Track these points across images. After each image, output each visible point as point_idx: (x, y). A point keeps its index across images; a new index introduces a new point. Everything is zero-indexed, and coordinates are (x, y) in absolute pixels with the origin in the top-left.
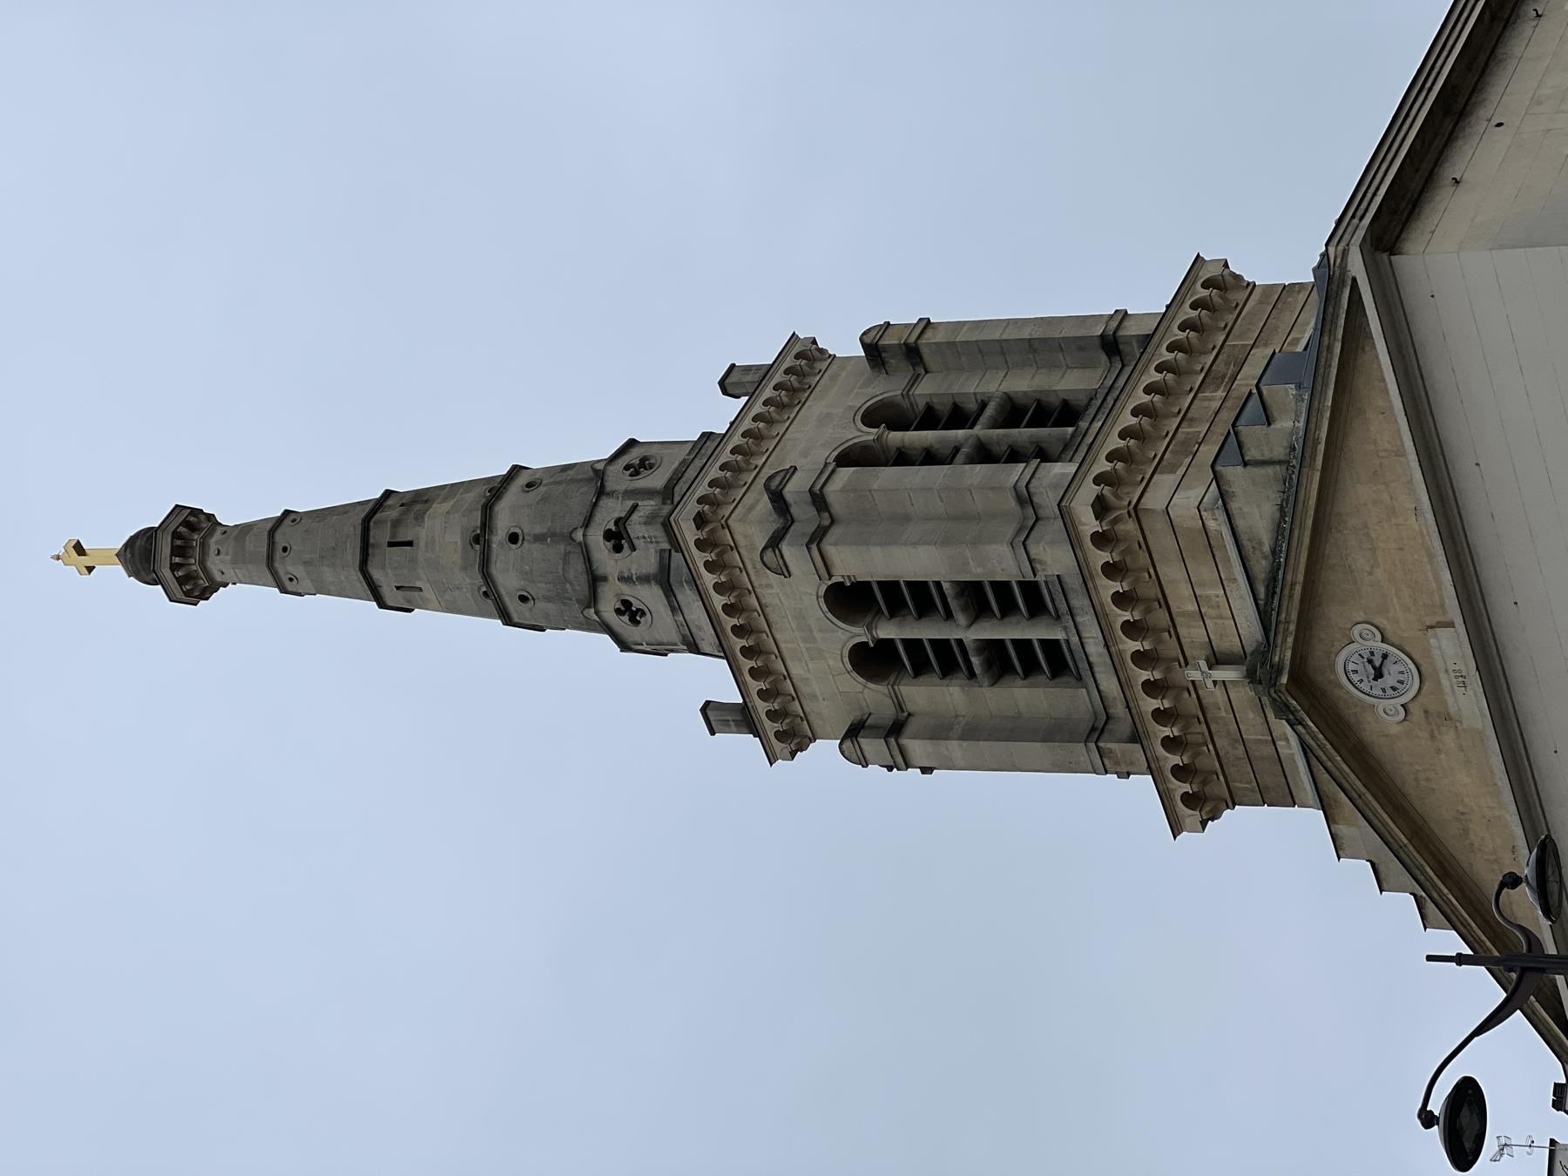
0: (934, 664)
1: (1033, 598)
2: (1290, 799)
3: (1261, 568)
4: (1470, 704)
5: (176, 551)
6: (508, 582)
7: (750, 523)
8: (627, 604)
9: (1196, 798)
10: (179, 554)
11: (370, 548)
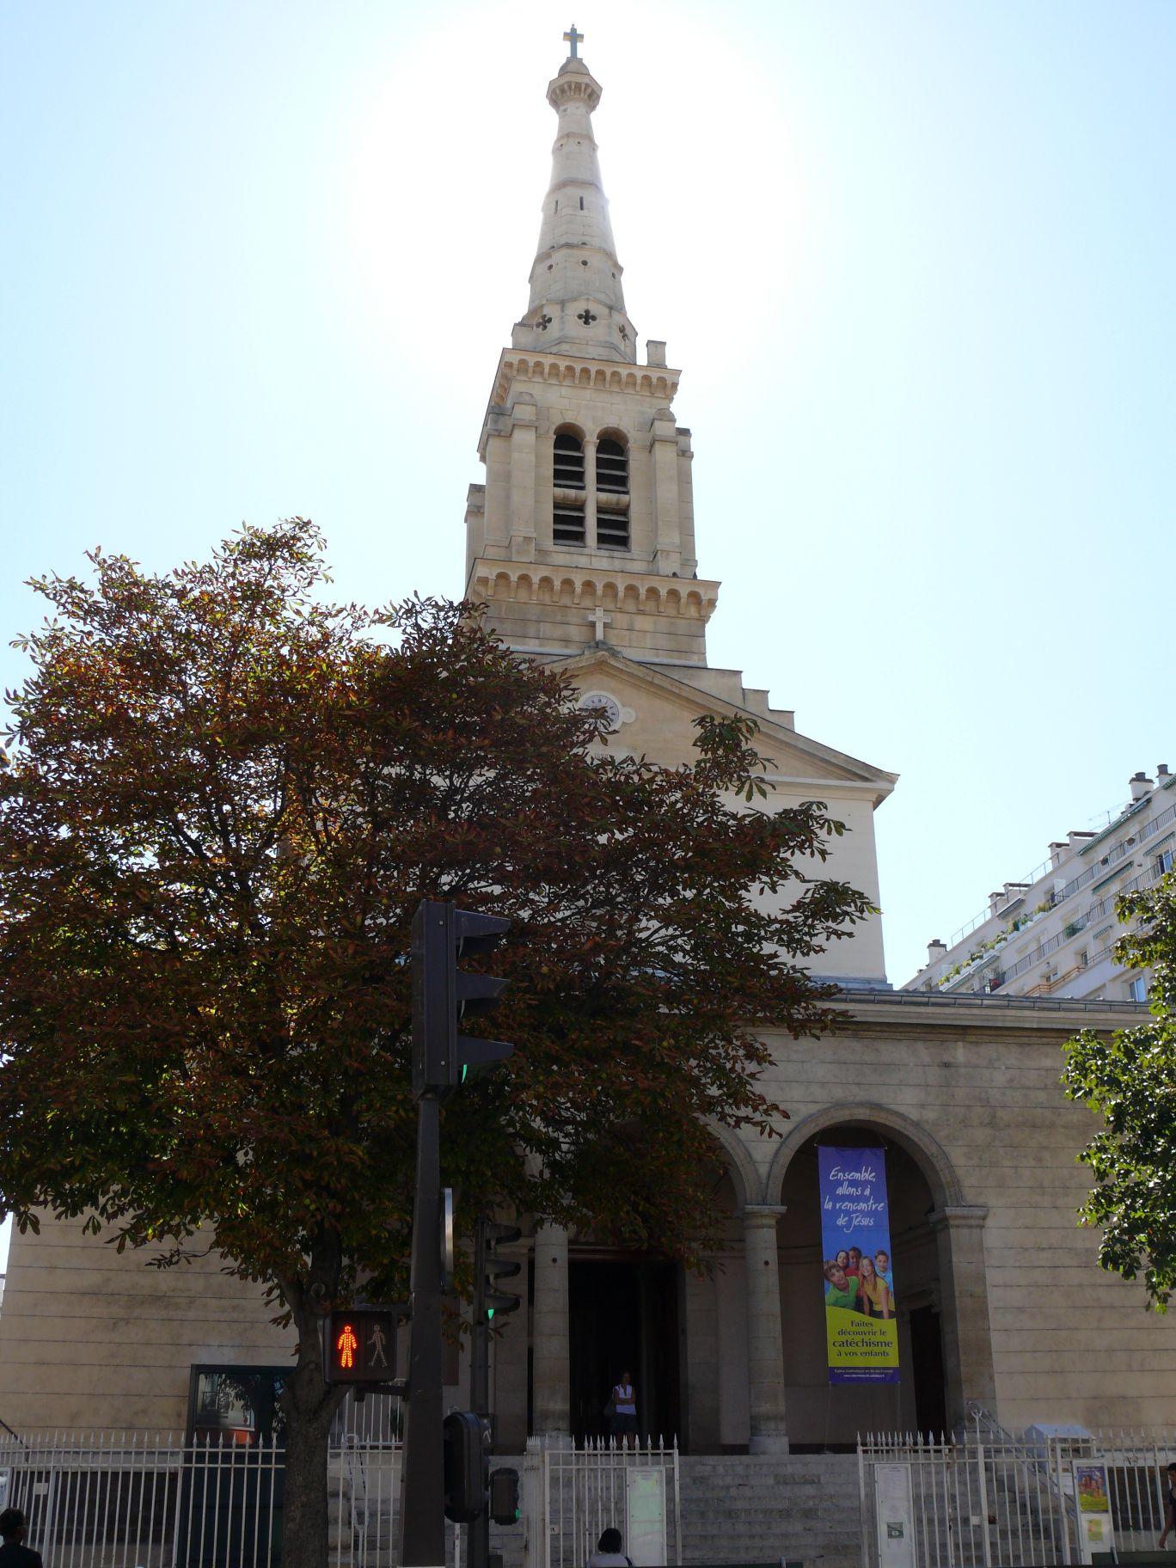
6: (558, 257)
8: (594, 318)
10: (574, 90)
11: (575, 186)
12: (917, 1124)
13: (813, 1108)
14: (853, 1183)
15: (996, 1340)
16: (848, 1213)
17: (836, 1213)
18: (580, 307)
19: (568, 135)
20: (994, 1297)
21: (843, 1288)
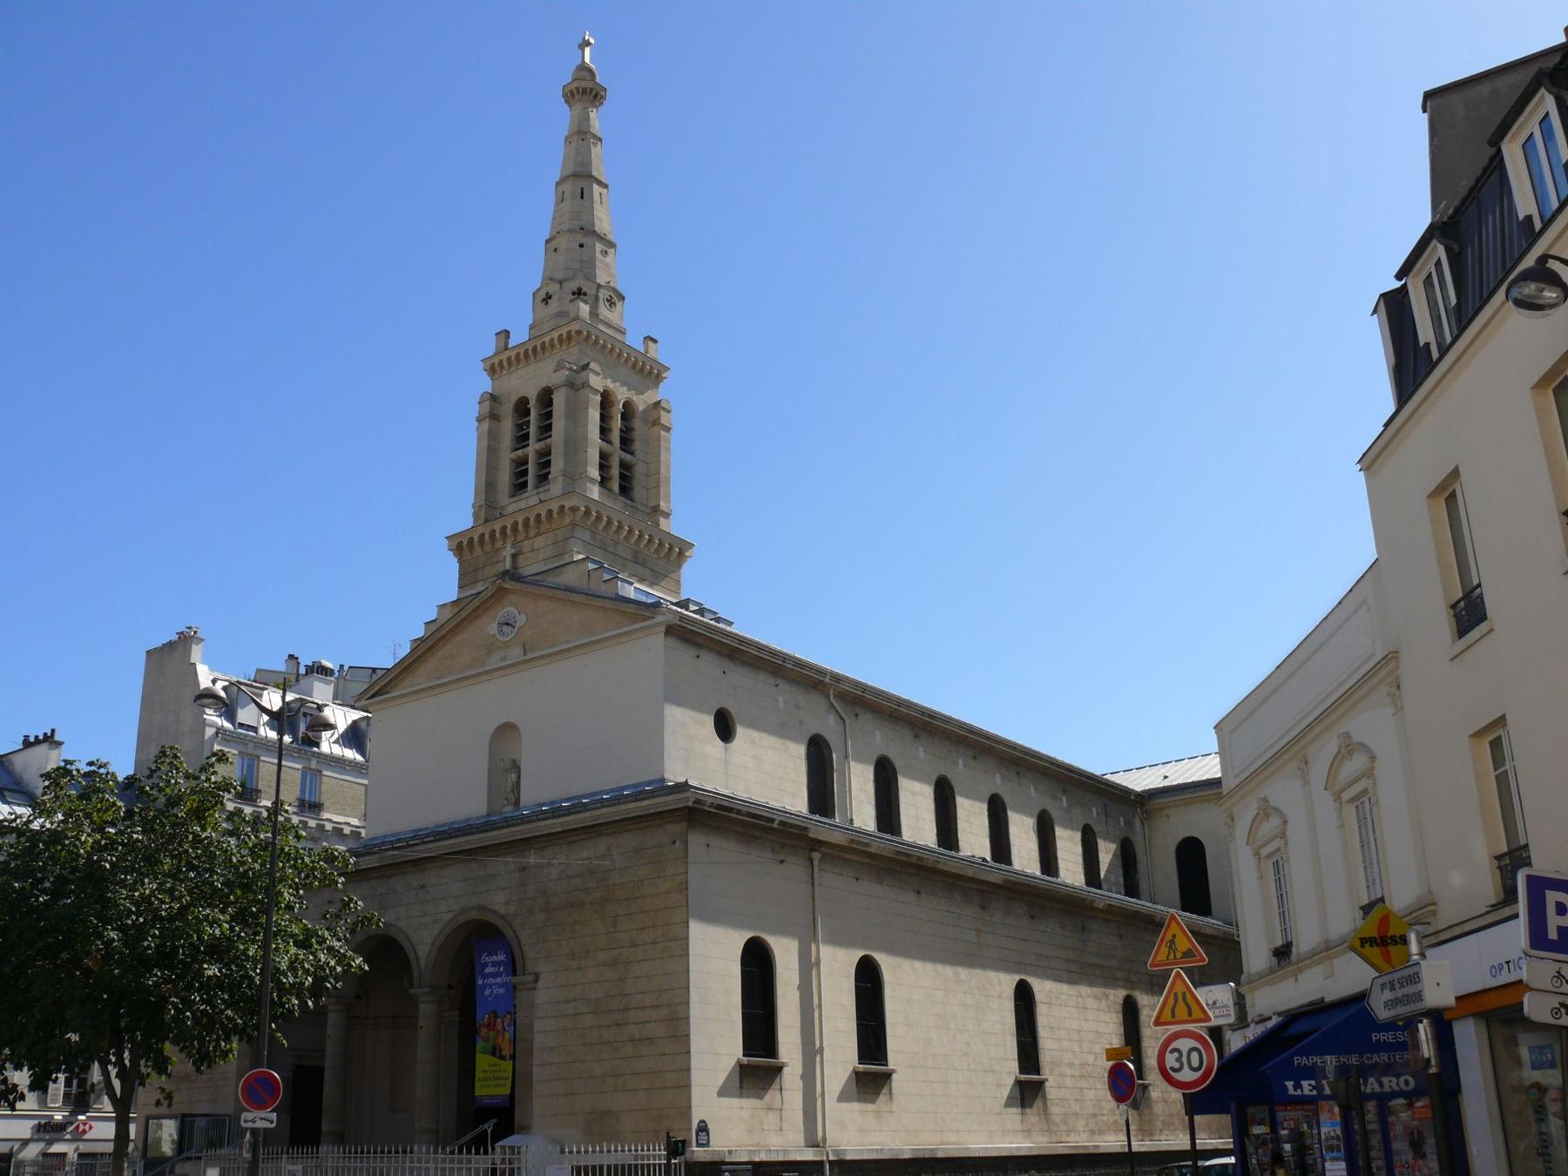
0: (522, 436)
1: (543, 478)
2: (462, 586)
3: (551, 579)
5: (584, 91)
7: (572, 354)
9: (462, 546)
11: (579, 181)
12: (503, 917)
13: (450, 916)
14: (495, 964)
16: (491, 986)
17: (484, 987)
18: (573, 286)
20: (539, 1040)
21: (486, 1040)
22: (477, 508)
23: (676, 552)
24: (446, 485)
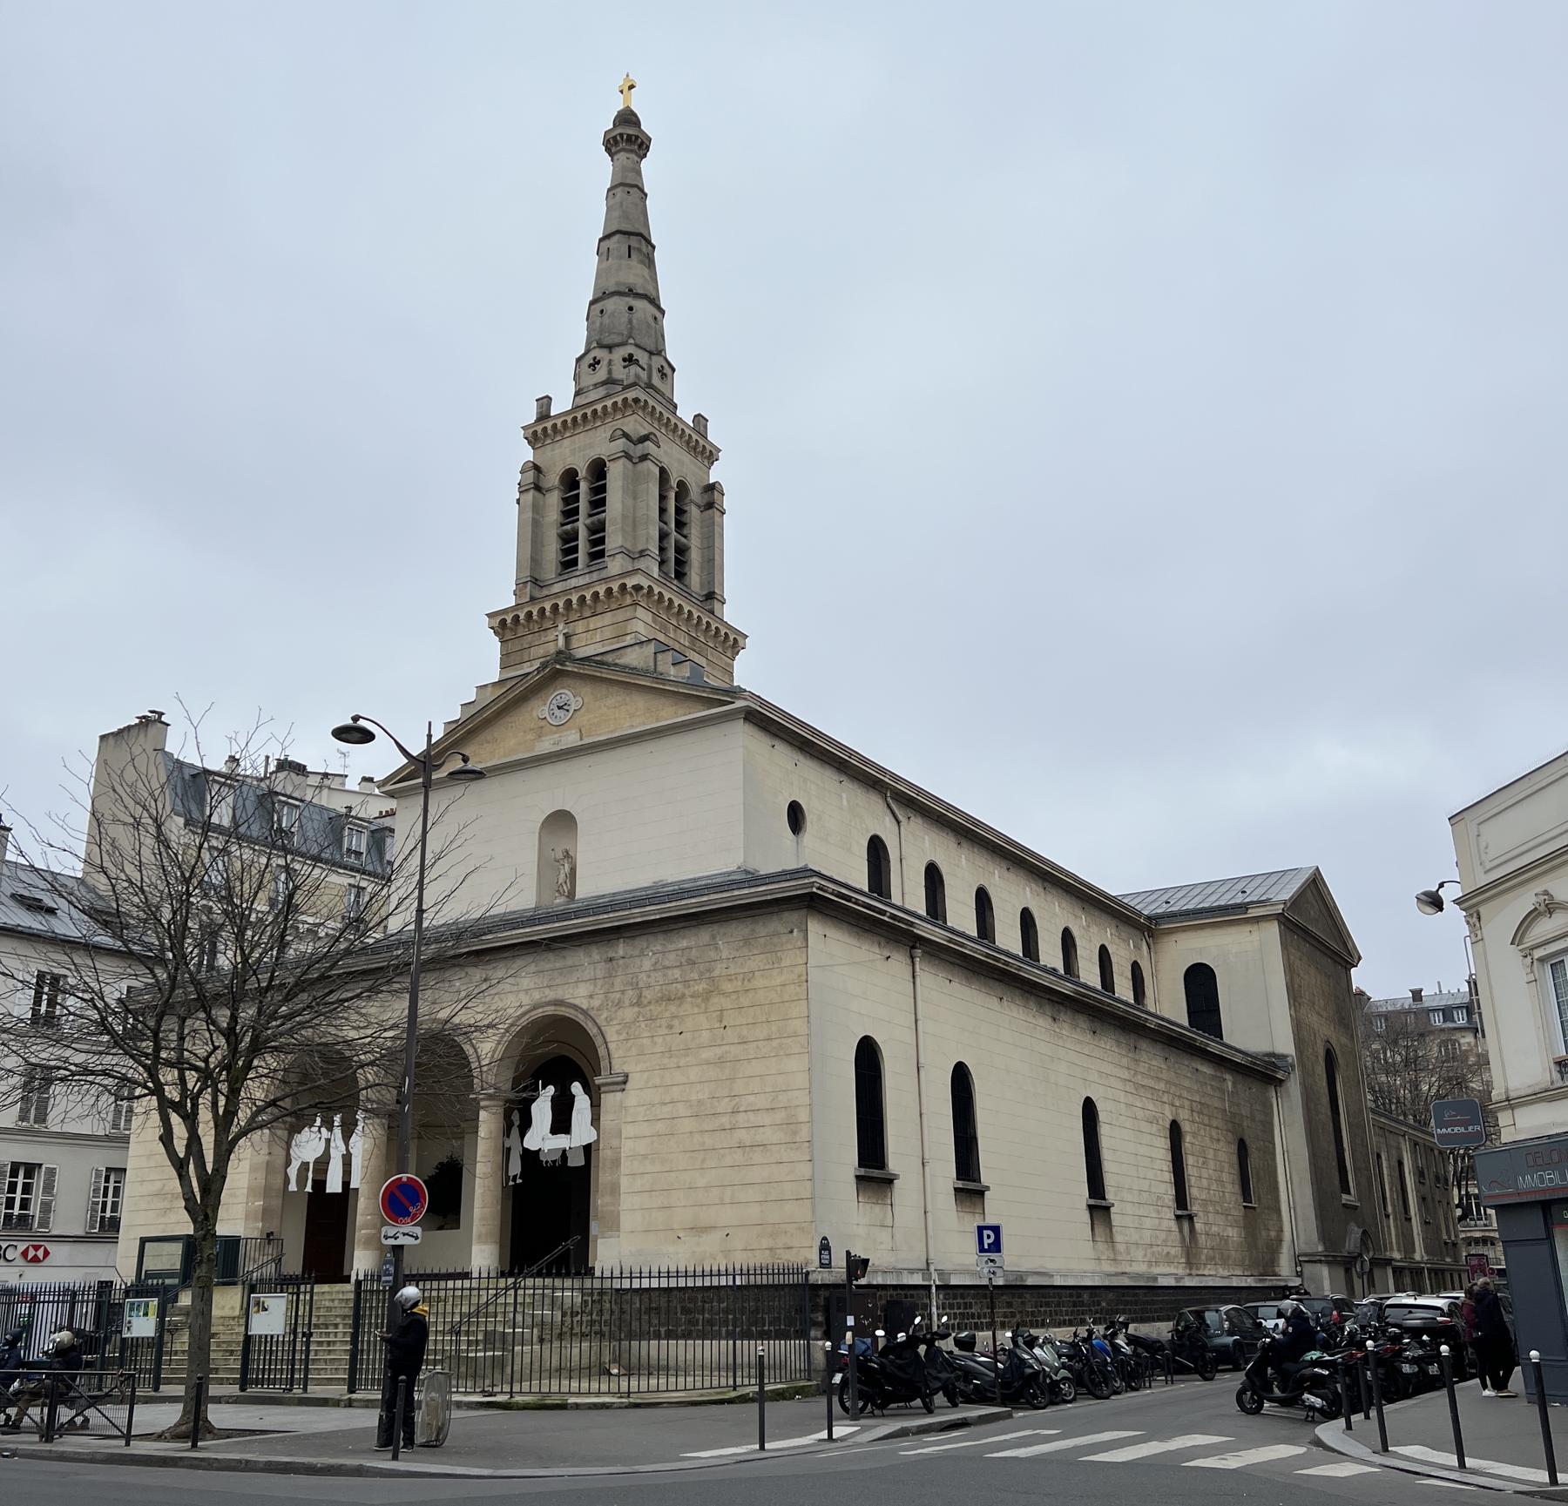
0: (570, 509)
3: (609, 658)
4: (546, 746)
7: (635, 424)
9: (504, 625)
10: (627, 138)
11: (628, 237)
12: (584, 1012)
15: (624, 1183)
19: (621, 184)
22: (521, 585)
23: (732, 642)
24: (488, 561)
